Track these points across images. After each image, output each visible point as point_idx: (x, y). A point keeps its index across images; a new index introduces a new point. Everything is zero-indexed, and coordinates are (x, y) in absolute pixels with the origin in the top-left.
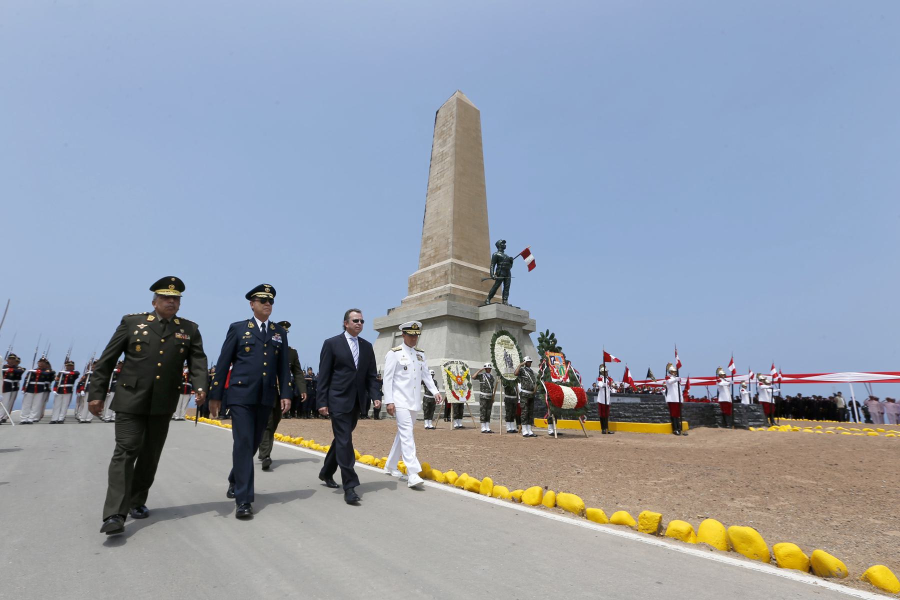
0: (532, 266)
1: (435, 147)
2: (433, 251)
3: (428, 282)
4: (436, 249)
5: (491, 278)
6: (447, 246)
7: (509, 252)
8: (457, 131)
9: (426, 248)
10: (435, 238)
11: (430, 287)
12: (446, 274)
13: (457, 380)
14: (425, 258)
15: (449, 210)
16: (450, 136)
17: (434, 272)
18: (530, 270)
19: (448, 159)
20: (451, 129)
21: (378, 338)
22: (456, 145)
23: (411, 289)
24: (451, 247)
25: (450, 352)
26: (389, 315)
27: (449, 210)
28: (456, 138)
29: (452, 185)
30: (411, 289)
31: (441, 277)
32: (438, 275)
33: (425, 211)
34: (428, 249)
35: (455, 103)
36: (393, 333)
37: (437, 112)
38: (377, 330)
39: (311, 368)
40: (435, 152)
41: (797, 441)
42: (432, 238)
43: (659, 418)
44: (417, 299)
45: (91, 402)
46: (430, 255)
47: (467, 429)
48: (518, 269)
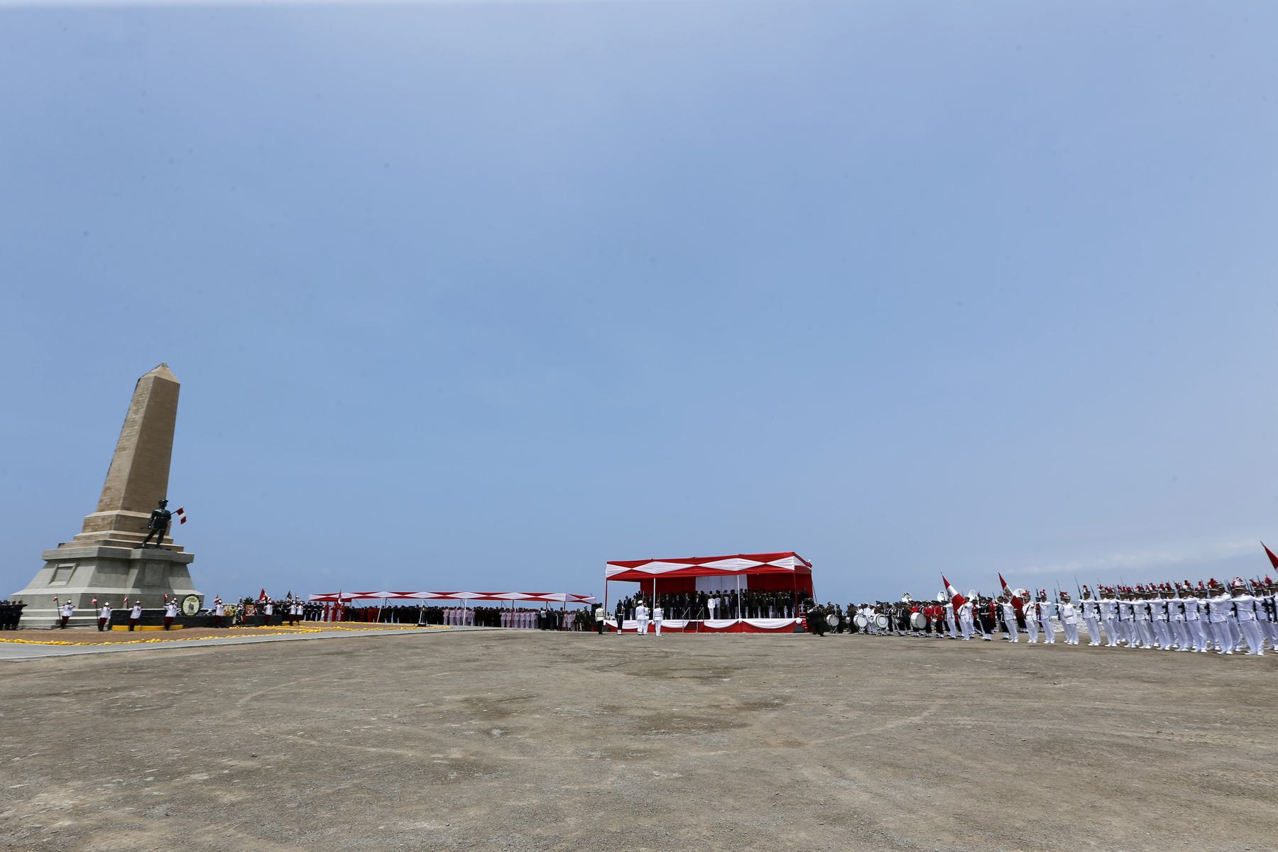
0: (183, 520)
1: (130, 412)
2: (109, 500)
3: (98, 525)
4: (112, 499)
6: (119, 500)
8: (148, 406)
9: (105, 496)
10: (112, 490)
12: (111, 522)
14: (102, 504)
16: (143, 407)
17: (104, 518)
18: (182, 523)
19: (136, 427)
20: (144, 402)
21: (44, 568)
22: (145, 418)
23: (85, 527)
24: (121, 501)
25: (93, 583)
28: (146, 412)
29: (134, 451)
30: (85, 527)
31: (108, 524)
32: (106, 522)
33: (111, 464)
34: (106, 497)
35: (152, 380)
36: (57, 565)
37: (139, 380)
38: (46, 560)
40: (129, 417)
42: (110, 489)
46: (106, 502)
47: (30, 637)
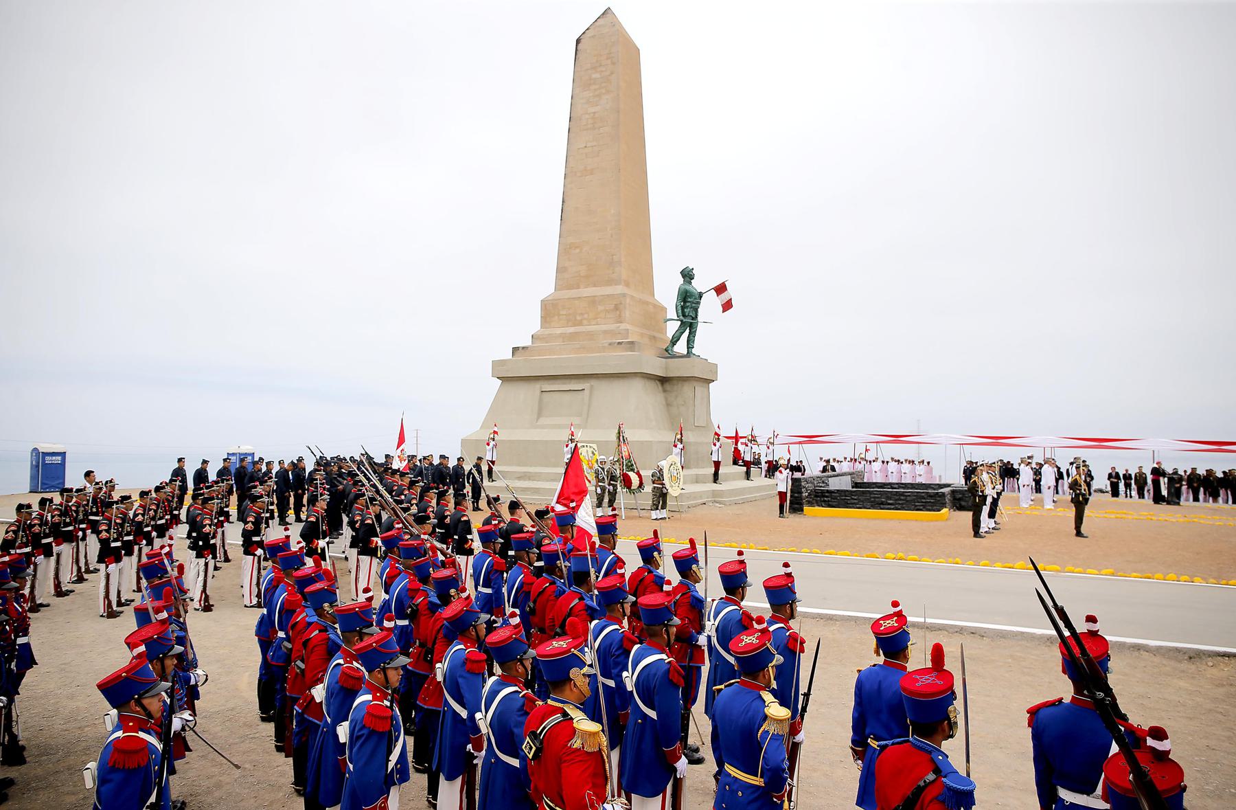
0: (727, 306)
5: (676, 318)
7: (698, 285)
11: (585, 322)
13: (588, 464)
15: (612, 211)
26: (1088, 535)
27: (612, 211)
39: (353, 457)
41: (1182, 675)
43: (922, 505)
44: (562, 336)
45: (987, 503)
48: (709, 306)
